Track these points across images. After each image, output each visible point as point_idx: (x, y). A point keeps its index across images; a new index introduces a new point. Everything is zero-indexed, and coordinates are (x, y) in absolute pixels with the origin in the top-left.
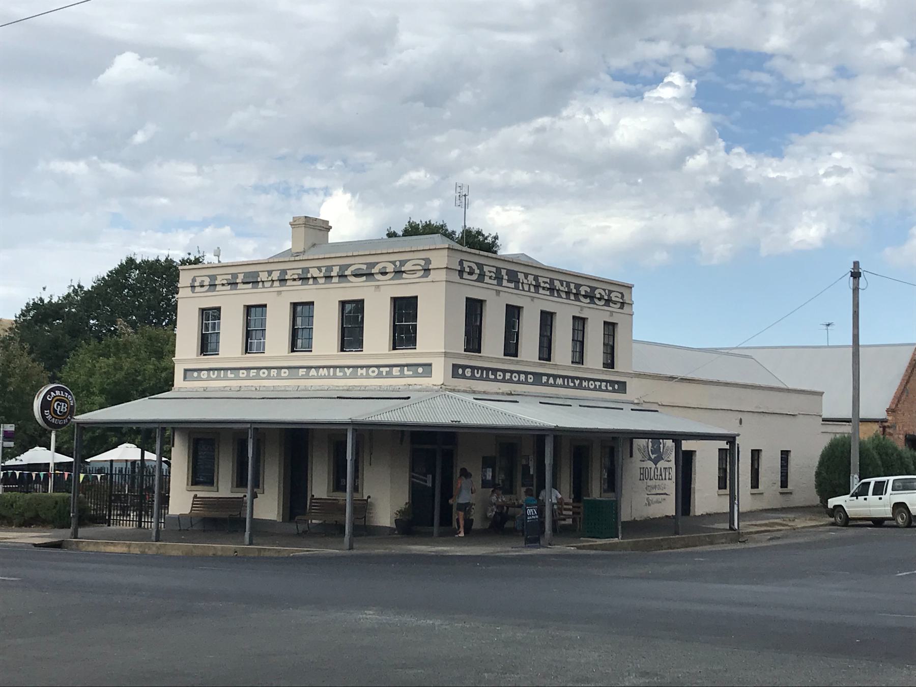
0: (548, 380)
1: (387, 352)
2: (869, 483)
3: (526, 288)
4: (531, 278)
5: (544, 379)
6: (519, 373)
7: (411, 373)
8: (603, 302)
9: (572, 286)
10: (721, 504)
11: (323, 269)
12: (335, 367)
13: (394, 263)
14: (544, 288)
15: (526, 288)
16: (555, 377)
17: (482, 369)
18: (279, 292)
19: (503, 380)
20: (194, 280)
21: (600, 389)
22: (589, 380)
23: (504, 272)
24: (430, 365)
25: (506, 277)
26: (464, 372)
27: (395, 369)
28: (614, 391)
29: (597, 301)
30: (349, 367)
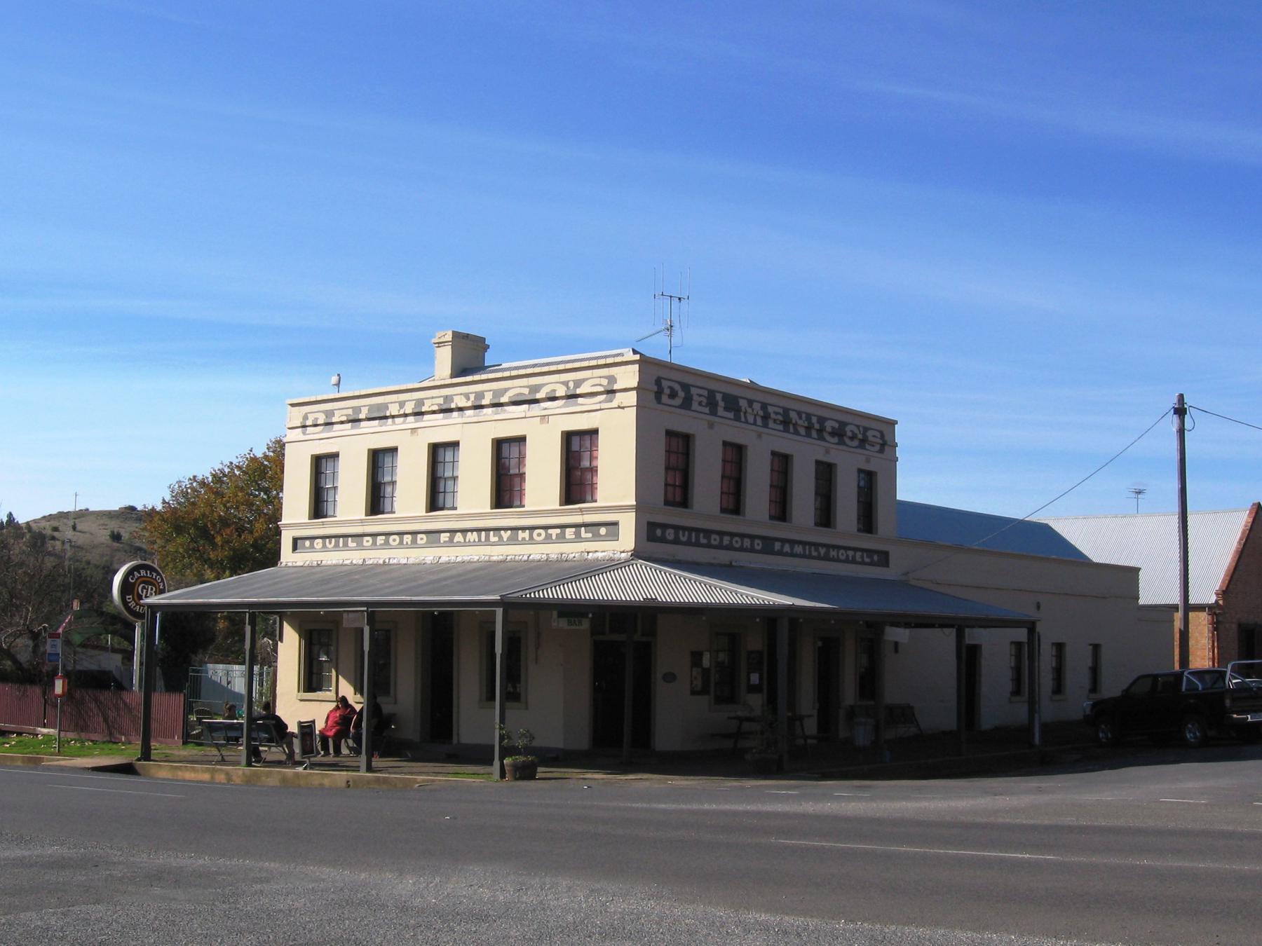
0: (782, 547)
1: (558, 507)
2: (1188, 679)
3: (751, 419)
4: (757, 406)
5: (777, 546)
6: (743, 536)
7: (590, 535)
8: (856, 443)
9: (814, 420)
10: (1018, 713)
11: (472, 397)
12: (487, 530)
13: (566, 384)
14: (775, 421)
15: (751, 419)
16: (793, 542)
17: (691, 530)
18: (414, 430)
19: (720, 547)
20: (306, 417)
21: (854, 562)
22: (838, 547)
23: (719, 397)
24: (616, 524)
25: (721, 404)
26: (663, 533)
27: (568, 530)
28: (872, 564)
29: (848, 441)
30: (506, 529)
